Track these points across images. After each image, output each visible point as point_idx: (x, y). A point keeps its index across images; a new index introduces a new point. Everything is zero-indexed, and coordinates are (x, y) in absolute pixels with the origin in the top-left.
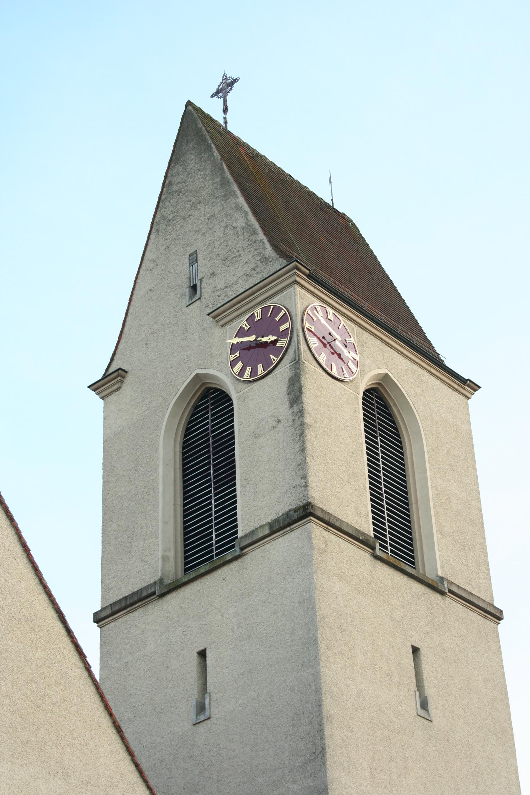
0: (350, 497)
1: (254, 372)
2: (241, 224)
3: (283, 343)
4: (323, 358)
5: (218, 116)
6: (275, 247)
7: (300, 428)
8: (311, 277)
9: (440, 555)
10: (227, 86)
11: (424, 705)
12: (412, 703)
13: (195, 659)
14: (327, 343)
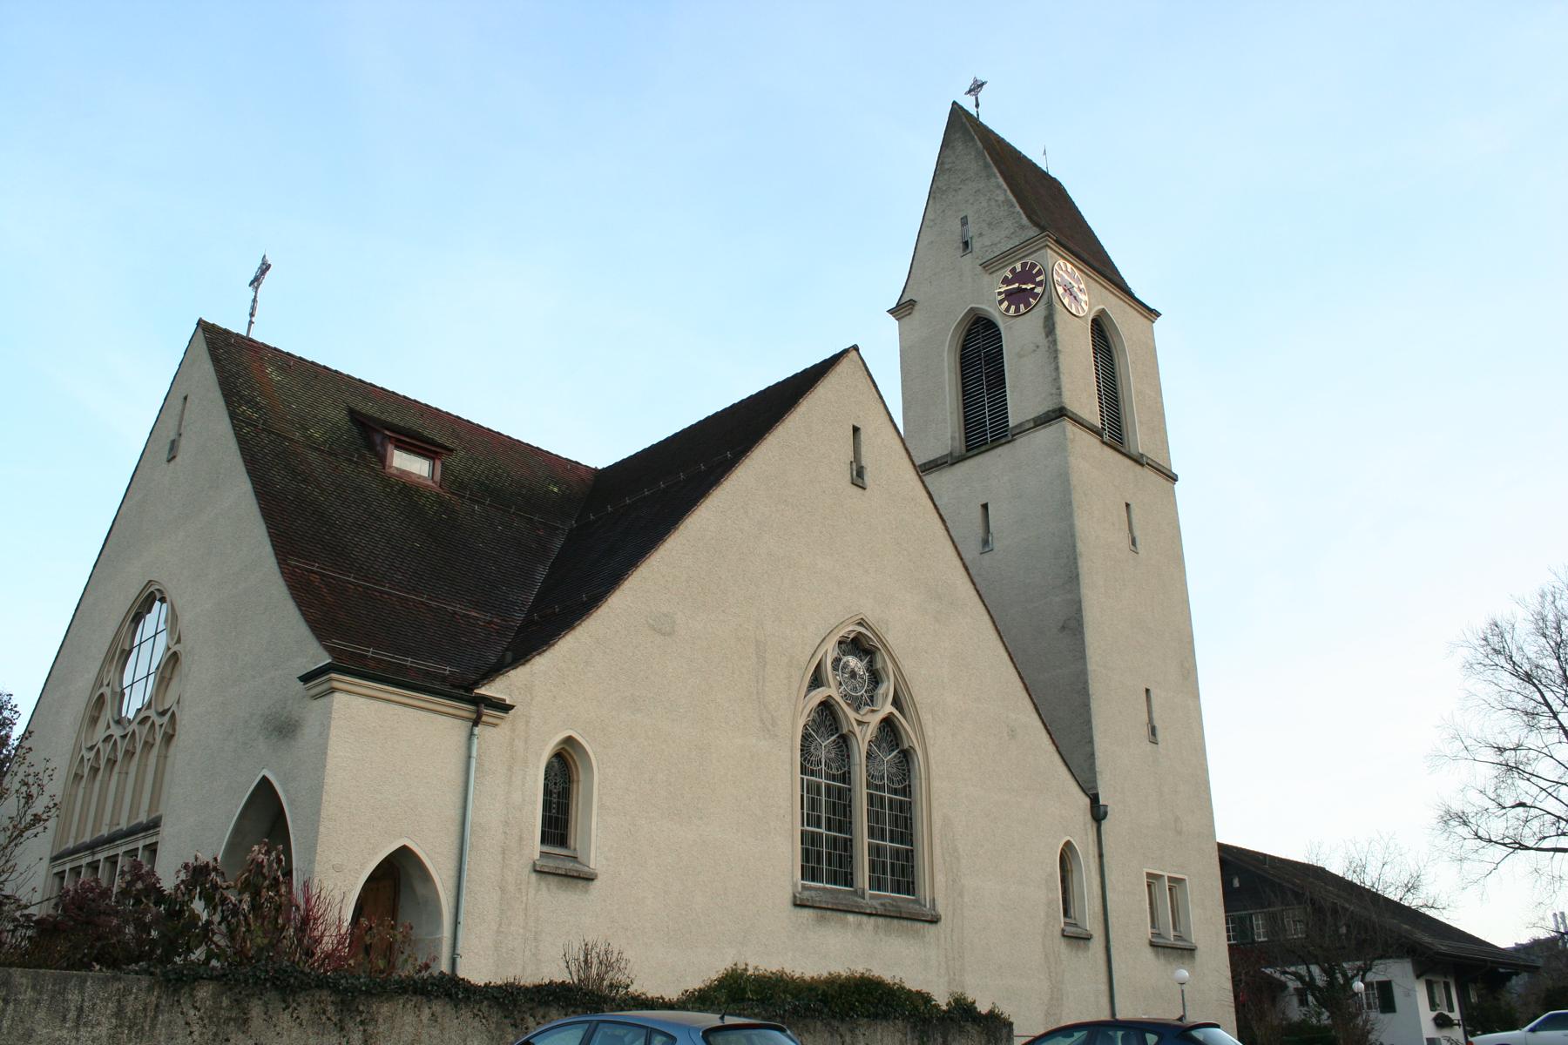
0: (1084, 399)
1: (1017, 310)
2: (1001, 198)
3: (1039, 290)
4: (1066, 302)
5: (973, 111)
6: (1029, 217)
7: (1054, 353)
8: (1057, 241)
9: (1141, 441)
10: (976, 87)
11: (1134, 542)
12: (1127, 542)
13: (979, 511)
14: (1068, 290)
